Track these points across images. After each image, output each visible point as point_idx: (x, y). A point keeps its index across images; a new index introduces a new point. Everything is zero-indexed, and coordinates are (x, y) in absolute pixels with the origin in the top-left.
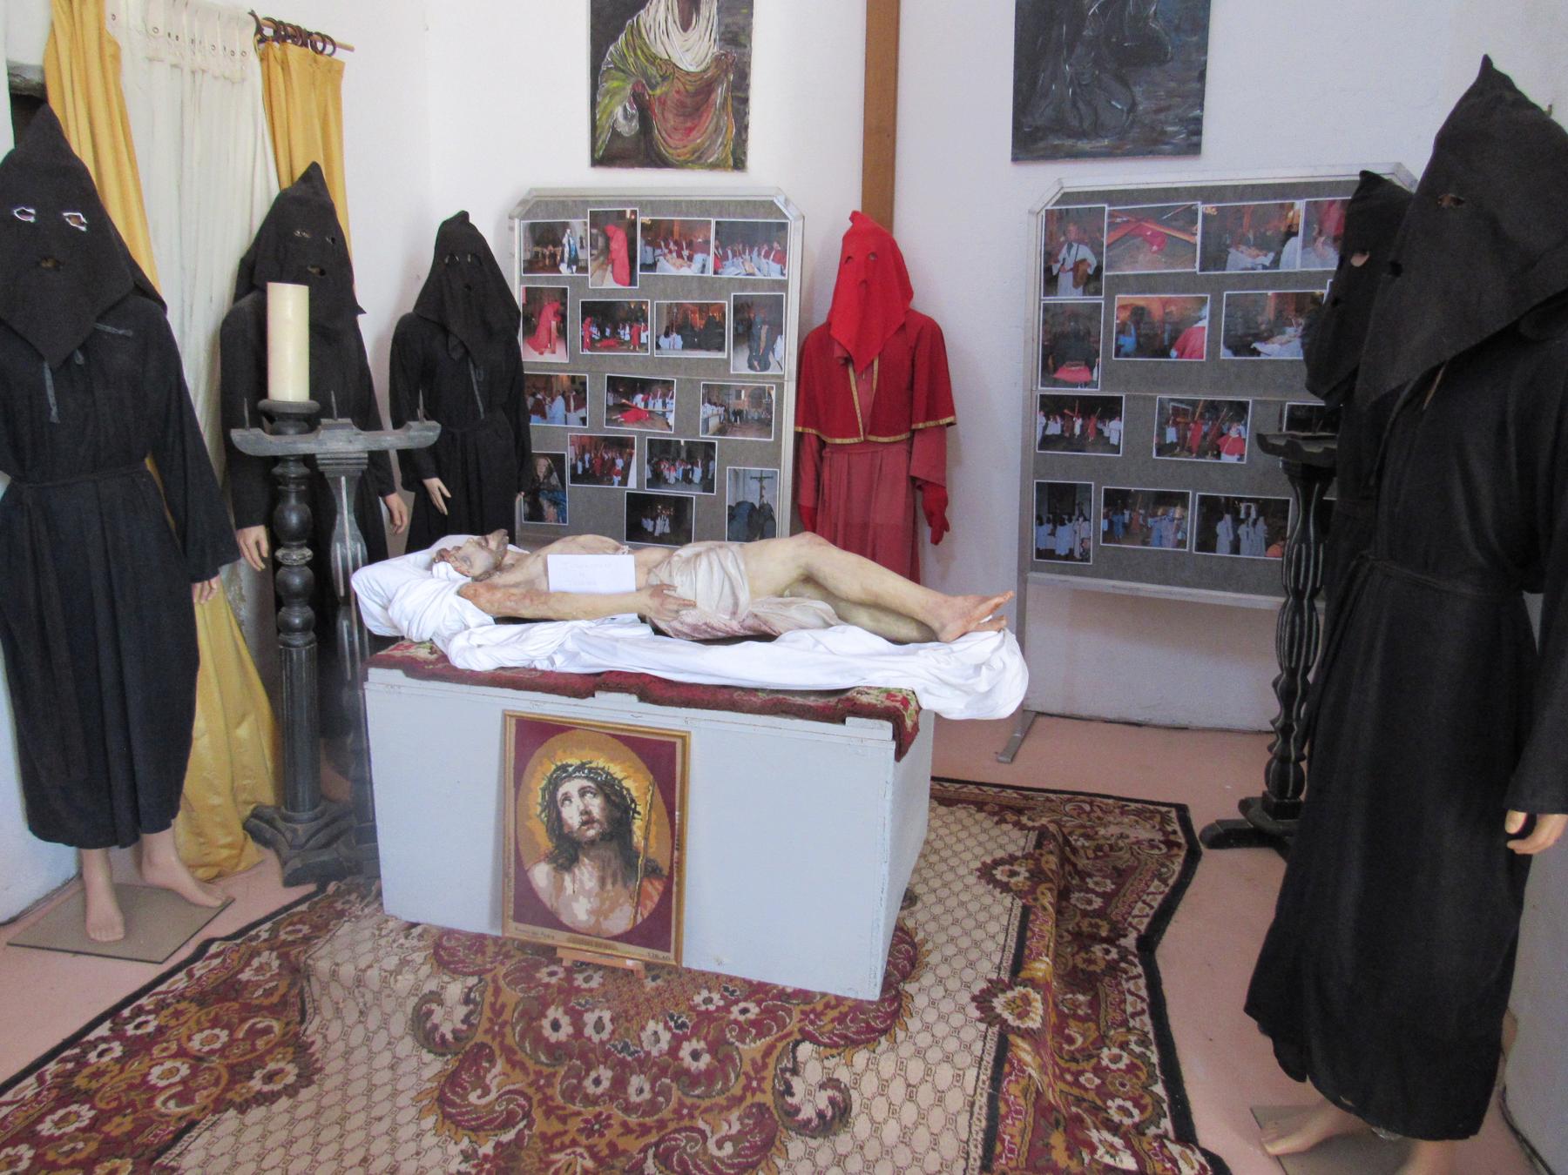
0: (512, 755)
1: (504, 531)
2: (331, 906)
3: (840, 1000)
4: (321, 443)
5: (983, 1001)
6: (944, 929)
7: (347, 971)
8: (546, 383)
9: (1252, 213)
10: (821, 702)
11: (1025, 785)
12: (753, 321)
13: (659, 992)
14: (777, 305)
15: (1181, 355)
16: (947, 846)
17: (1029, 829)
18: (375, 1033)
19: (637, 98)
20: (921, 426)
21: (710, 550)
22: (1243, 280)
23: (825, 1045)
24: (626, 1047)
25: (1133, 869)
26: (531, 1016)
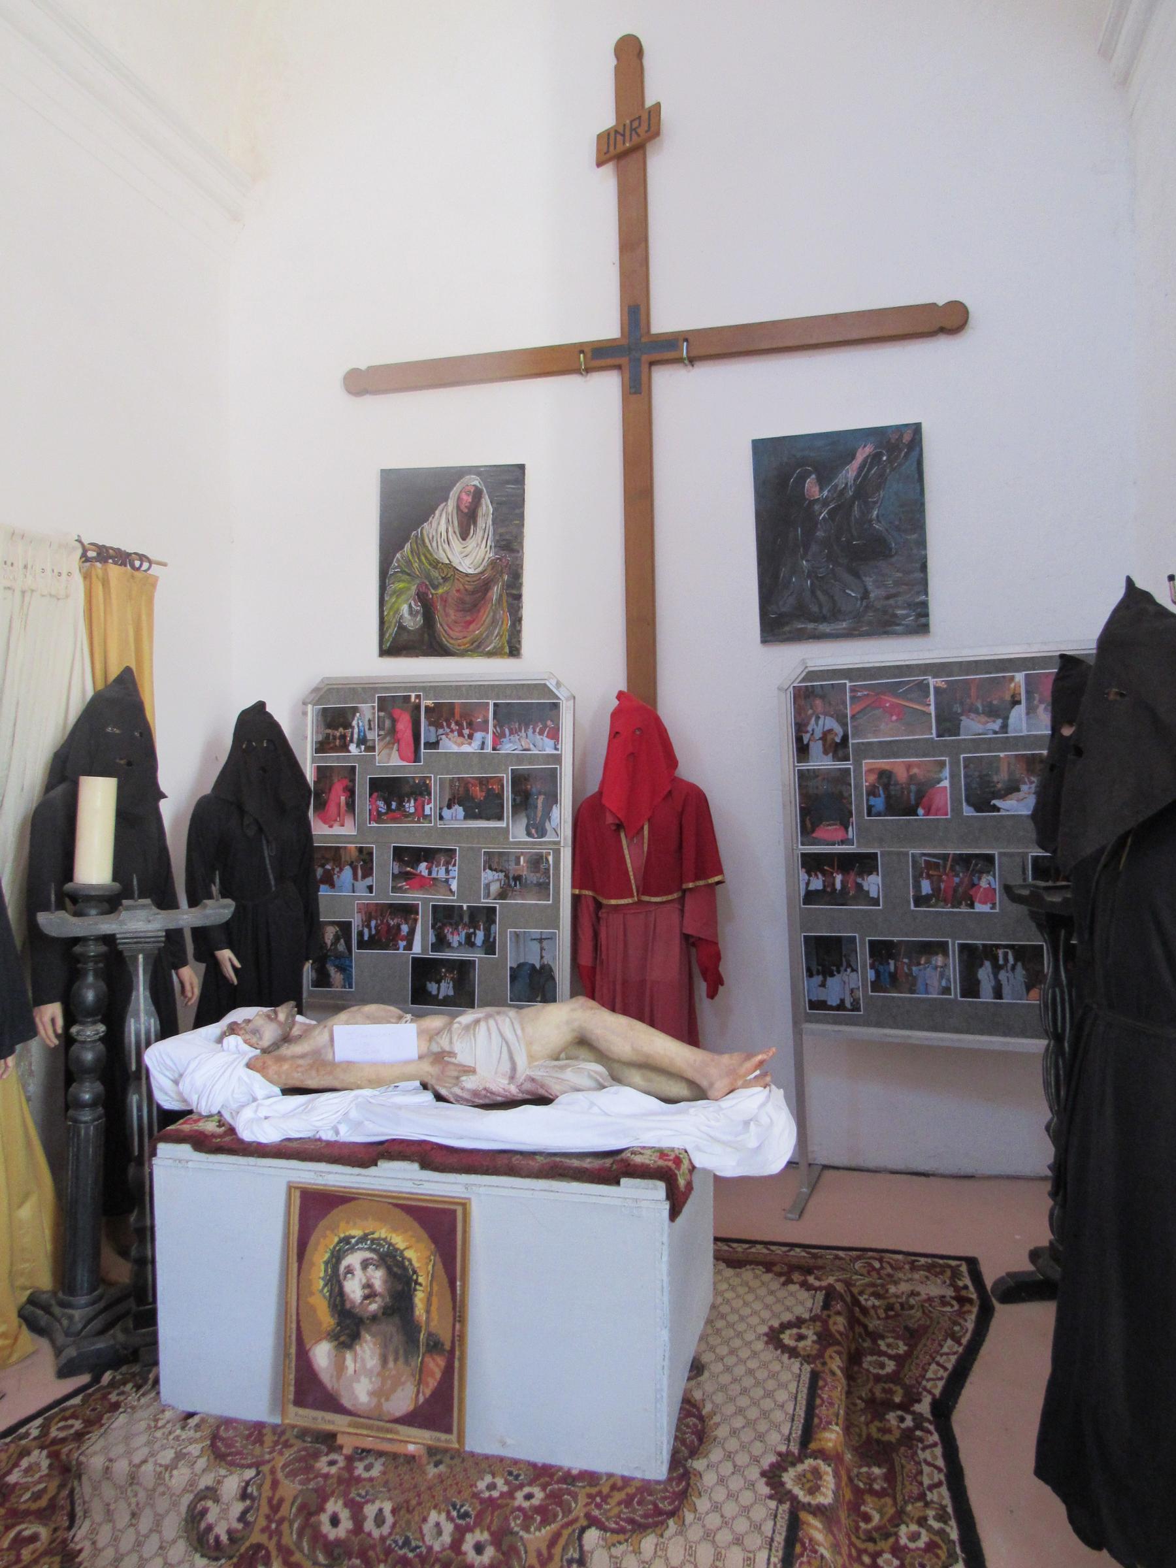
0: (295, 1228)
1: (292, 1003)
2: (105, 1397)
3: (627, 1481)
4: (123, 923)
5: (773, 1476)
6: (732, 1399)
7: (121, 1467)
8: (335, 855)
9: (971, 688)
10: (597, 1163)
11: (814, 1242)
12: (530, 791)
13: (441, 1478)
14: (552, 777)
15: (927, 813)
16: (733, 1310)
17: (816, 1289)
18: (147, 1536)
19: (422, 597)
20: (691, 885)
21: (488, 1017)
22: (977, 744)
23: (613, 1531)
24: (407, 1542)
25: (926, 1329)
26: (309, 1510)
